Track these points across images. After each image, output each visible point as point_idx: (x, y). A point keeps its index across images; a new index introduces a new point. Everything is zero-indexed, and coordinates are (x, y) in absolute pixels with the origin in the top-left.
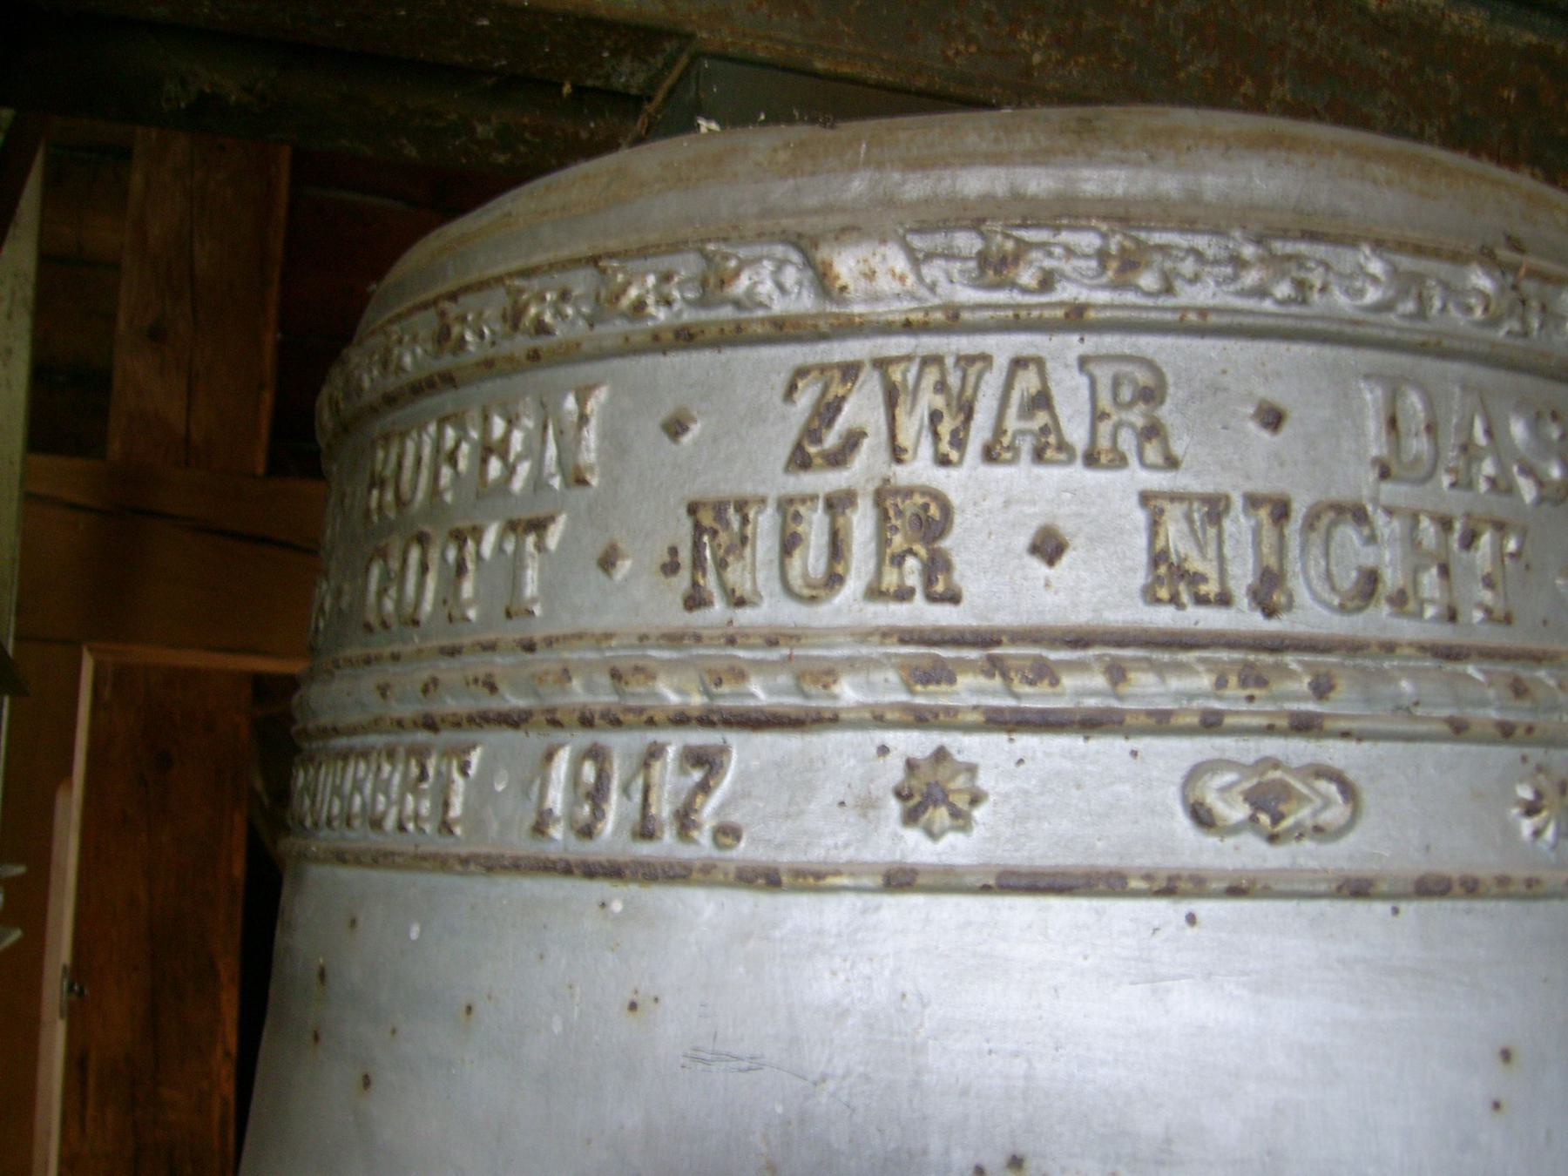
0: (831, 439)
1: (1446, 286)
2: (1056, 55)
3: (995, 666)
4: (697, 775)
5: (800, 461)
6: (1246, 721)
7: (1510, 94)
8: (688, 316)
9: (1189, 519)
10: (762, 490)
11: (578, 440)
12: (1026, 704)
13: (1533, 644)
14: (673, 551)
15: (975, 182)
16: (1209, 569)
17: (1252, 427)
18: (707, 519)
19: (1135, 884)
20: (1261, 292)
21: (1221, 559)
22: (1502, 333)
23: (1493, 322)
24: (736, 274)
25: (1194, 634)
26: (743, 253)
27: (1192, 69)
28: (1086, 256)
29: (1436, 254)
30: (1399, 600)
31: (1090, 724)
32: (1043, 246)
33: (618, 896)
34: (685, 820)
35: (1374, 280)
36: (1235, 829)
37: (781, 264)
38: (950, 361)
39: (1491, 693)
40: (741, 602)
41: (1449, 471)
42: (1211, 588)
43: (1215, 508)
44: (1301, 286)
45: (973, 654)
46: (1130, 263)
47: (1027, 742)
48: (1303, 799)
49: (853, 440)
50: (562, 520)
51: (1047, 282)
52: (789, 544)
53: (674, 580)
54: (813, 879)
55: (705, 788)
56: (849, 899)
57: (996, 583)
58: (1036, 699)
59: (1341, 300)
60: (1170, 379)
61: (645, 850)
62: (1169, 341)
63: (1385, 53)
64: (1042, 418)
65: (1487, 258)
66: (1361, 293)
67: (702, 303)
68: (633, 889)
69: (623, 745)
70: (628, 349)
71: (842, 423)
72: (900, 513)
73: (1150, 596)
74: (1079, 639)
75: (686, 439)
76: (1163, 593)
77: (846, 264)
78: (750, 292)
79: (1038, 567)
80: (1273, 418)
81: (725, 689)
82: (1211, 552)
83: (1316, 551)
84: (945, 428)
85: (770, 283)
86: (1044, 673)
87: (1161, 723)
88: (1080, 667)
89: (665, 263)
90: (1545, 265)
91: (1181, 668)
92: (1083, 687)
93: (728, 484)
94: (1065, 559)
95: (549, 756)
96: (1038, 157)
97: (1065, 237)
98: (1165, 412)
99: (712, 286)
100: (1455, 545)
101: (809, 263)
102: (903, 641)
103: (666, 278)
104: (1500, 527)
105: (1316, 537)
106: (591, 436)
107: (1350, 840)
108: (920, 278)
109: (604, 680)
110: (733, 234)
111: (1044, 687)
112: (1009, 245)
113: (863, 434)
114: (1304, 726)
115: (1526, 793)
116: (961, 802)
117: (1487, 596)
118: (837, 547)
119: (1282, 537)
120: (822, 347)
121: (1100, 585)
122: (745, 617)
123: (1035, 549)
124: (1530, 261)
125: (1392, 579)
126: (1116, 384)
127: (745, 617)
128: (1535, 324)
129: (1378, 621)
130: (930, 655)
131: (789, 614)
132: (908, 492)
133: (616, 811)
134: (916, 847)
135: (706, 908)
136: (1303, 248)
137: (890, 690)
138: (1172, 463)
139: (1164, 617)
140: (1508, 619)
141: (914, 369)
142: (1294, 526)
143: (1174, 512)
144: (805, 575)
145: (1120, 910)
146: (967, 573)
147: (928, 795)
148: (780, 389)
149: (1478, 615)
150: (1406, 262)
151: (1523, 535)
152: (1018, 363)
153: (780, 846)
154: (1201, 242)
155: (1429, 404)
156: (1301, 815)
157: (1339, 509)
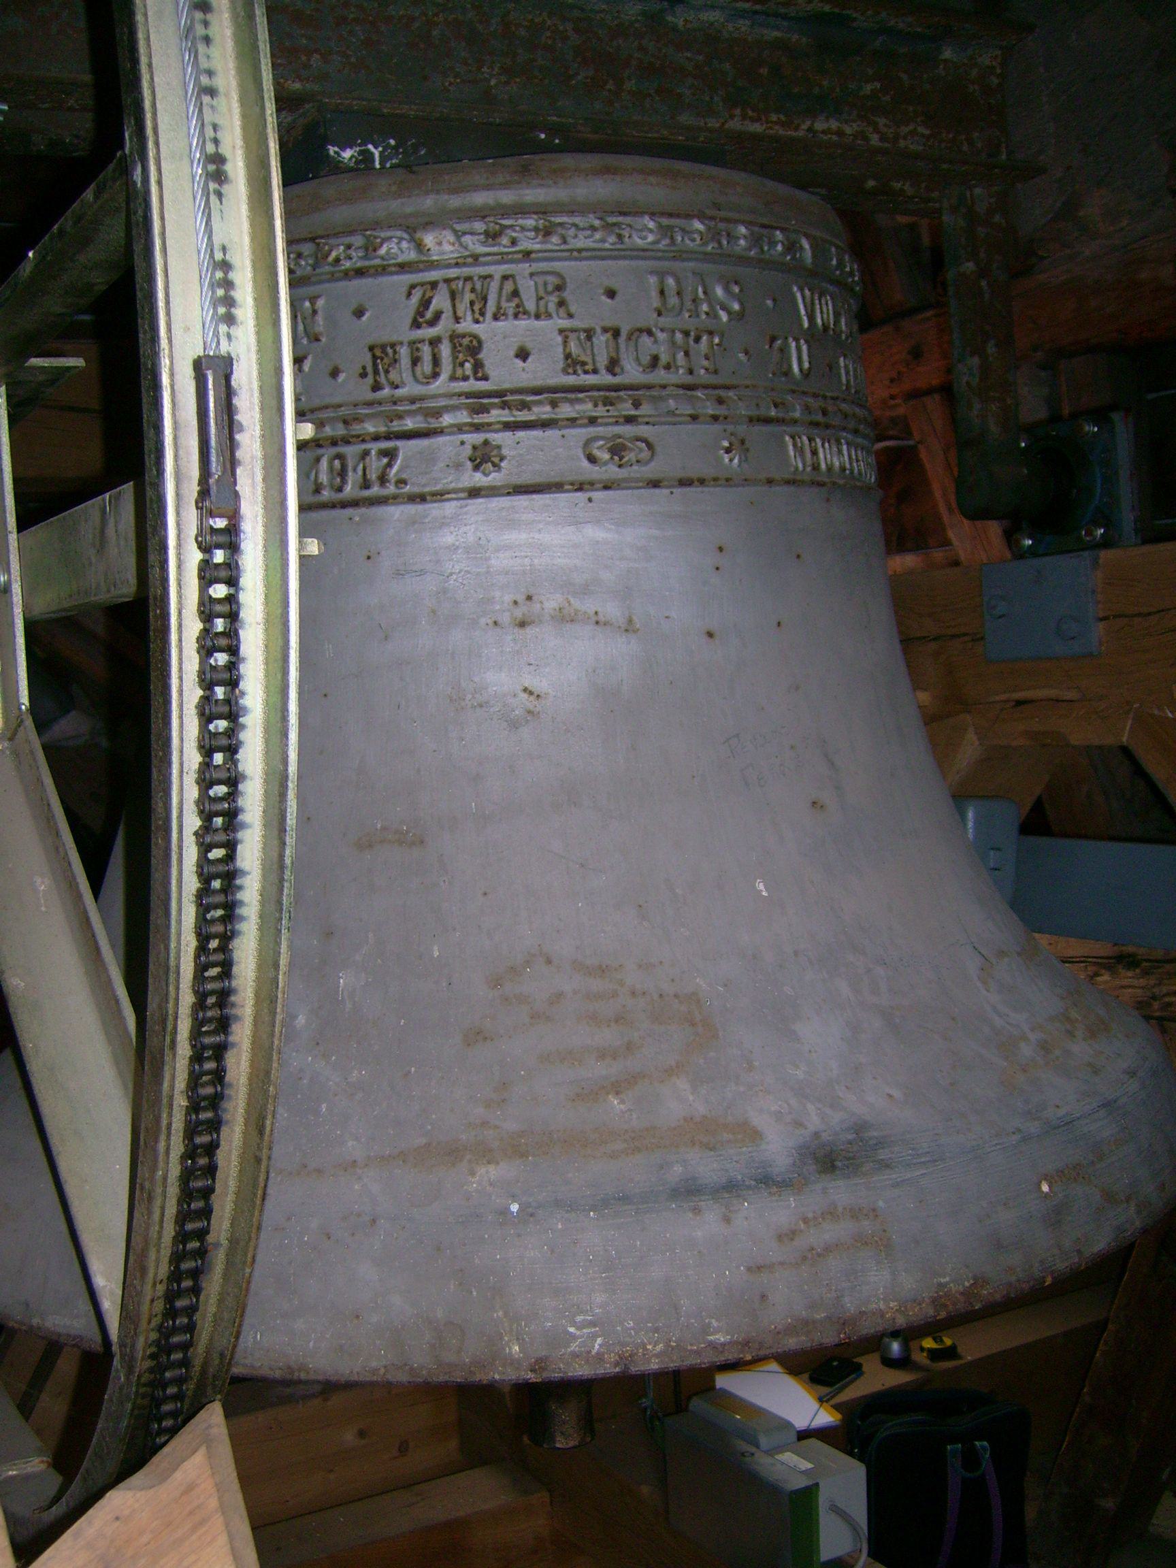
0: (429, 315)
1: (683, 230)
2: (503, 78)
3: (505, 405)
4: (385, 460)
5: (416, 325)
6: (606, 420)
7: (764, 71)
8: (359, 264)
9: (579, 339)
10: (400, 339)
11: (313, 322)
12: (519, 419)
13: (728, 382)
14: (364, 368)
15: (480, 199)
16: (588, 359)
17: (603, 298)
18: (378, 353)
19: (567, 487)
20: (603, 241)
21: (593, 355)
22: (710, 248)
23: (705, 244)
24: (381, 244)
25: (585, 386)
26: (383, 235)
27: (579, 78)
28: (529, 230)
29: (678, 216)
30: (668, 367)
31: (545, 424)
32: (511, 226)
33: (356, 514)
34: (383, 480)
35: (651, 231)
36: (606, 463)
37: (401, 239)
38: (476, 278)
39: (708, 403)
40: (397, 387)
41: (689, 311)
42: (589, 367)
43: (590, 333)
44: (620, 237)
45: (496, 400)
46: (547, 233)
47: (521, 434)
48: (631, 450)
49: (438, 316)
50: (310, 358)
51: (514, 242)
52: (415, 361)
53: (366, 380)
54: (440, 496)
55: (389, 465)
56: (454, 503)
57: (503, 371)
58: (523, 416)
59: (639, 241)
60: (568, 280)
61: (366, 493)
62: (567, 263)
63: (689, 55)
64: (516, 301)
65: (701, 217)
66: (645, 238)
67: (366, 257)
68: (363, 510)
69: (351, 451)
70: (333, 278)
71: (432, 308)
72: (461, 345)
73: (565, 372)
74: (537, 391)
75: (364, 318)
76: (570, 370)
77: (429, 239)
78: (388, 253)
79: (519, 362)
80: (611, 294)
81: (395, 423)
82: (589, 352)
83: (632, 349)
84: (477, 307)
85: (396, 248)
86: (525, 406)
87: (572, 422)
88: (539, 403)
89: (348, 240)
90: (730, 215)
91: (578, 401)
92: (543, 411)
93: (386, 337)
94: (530, 360)
95: (318, 460)
96: (505, 185)
97: (520, 222)
98: (566, 294)
99: (370, 248)
100: (692, 342)
101: (412, 240)
102: (467, 398)
103: (349, 247)
104: (711, 333)
105: (632, 343)
106: (320, 319)
107: (653, 464)
108: (461, 245)
109: (341, 425)
110: (377, 225)
111: (525, 412)
112: (497, 227)
113: (442, 312)
114: (630, 420)
115: (726, 444)
116: (496, 460)
117: (706, 363)
118: (436, 361)
119: (617, 344)
120: (421, 274)
121: (544, 369)
122: (400, 392)
123: (517, 356)
124: (723, 214)
125: (664, 358)
126: (545, 284)
127: (400, 392)
128: (725, 242)
129: (660, 376)
130: (478, 403)
131: (418, 390)
132: (464, 336)
133: (353, 479)
134: (479, 479)
135: (395, 512)
136: (620, 219)
137: (463, 417)
138: (570, 316)
139: (571, 380)
140: (716, 372)
141: (460, 285)
142: (622, 339)
143: (572, 336)
144: (423, 373)
145: (562, 497)
146: (490, 368)
147: (483, 457)
148: (404, 295)
149: (702, 371)
150: (665, 221)
151: (722, 336)
152: (505, 278)
153: (424, 486)
154: (577, 220)
155: (678, 281)
156: (630, 456)
157: (640, 331)
